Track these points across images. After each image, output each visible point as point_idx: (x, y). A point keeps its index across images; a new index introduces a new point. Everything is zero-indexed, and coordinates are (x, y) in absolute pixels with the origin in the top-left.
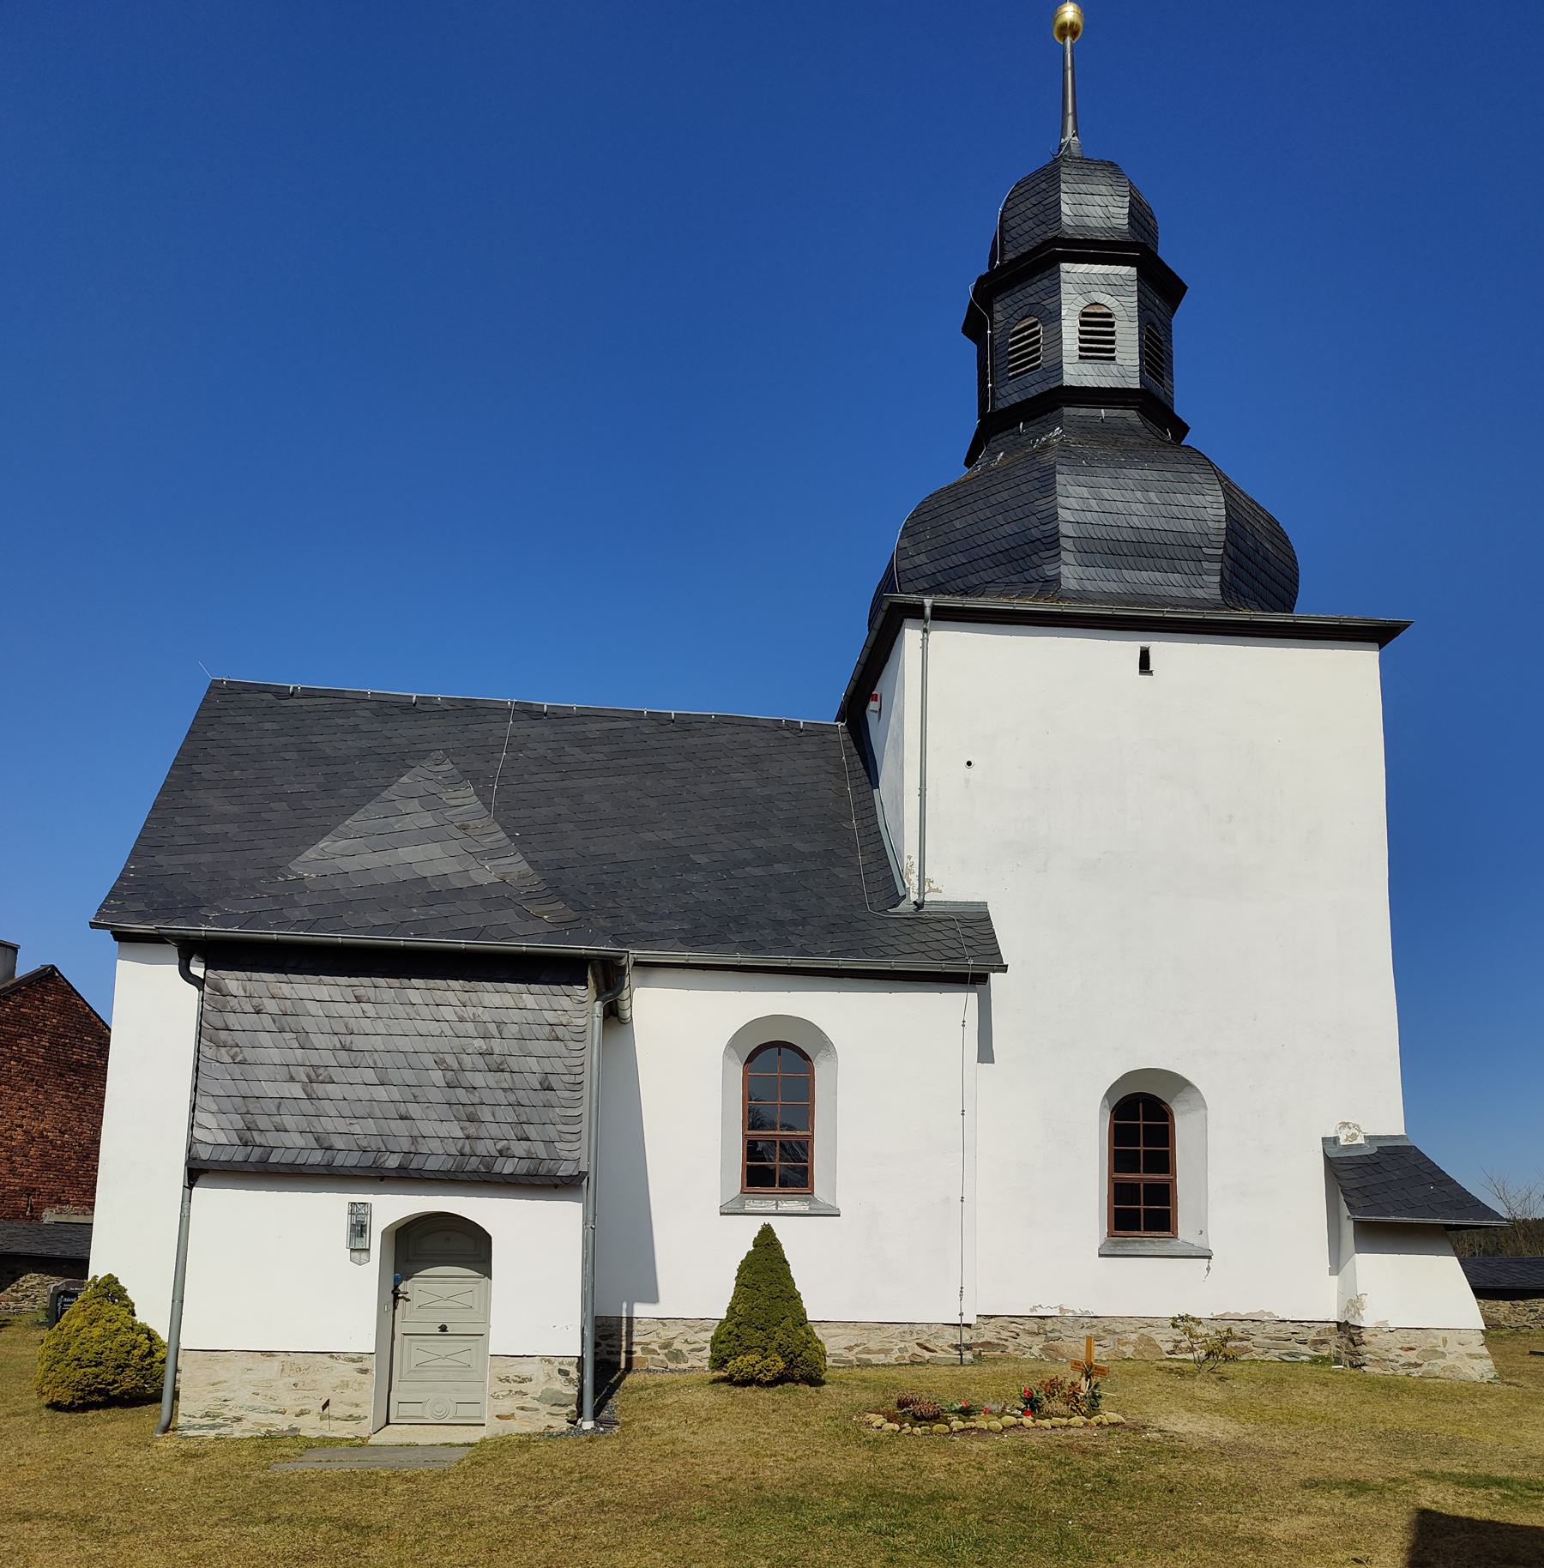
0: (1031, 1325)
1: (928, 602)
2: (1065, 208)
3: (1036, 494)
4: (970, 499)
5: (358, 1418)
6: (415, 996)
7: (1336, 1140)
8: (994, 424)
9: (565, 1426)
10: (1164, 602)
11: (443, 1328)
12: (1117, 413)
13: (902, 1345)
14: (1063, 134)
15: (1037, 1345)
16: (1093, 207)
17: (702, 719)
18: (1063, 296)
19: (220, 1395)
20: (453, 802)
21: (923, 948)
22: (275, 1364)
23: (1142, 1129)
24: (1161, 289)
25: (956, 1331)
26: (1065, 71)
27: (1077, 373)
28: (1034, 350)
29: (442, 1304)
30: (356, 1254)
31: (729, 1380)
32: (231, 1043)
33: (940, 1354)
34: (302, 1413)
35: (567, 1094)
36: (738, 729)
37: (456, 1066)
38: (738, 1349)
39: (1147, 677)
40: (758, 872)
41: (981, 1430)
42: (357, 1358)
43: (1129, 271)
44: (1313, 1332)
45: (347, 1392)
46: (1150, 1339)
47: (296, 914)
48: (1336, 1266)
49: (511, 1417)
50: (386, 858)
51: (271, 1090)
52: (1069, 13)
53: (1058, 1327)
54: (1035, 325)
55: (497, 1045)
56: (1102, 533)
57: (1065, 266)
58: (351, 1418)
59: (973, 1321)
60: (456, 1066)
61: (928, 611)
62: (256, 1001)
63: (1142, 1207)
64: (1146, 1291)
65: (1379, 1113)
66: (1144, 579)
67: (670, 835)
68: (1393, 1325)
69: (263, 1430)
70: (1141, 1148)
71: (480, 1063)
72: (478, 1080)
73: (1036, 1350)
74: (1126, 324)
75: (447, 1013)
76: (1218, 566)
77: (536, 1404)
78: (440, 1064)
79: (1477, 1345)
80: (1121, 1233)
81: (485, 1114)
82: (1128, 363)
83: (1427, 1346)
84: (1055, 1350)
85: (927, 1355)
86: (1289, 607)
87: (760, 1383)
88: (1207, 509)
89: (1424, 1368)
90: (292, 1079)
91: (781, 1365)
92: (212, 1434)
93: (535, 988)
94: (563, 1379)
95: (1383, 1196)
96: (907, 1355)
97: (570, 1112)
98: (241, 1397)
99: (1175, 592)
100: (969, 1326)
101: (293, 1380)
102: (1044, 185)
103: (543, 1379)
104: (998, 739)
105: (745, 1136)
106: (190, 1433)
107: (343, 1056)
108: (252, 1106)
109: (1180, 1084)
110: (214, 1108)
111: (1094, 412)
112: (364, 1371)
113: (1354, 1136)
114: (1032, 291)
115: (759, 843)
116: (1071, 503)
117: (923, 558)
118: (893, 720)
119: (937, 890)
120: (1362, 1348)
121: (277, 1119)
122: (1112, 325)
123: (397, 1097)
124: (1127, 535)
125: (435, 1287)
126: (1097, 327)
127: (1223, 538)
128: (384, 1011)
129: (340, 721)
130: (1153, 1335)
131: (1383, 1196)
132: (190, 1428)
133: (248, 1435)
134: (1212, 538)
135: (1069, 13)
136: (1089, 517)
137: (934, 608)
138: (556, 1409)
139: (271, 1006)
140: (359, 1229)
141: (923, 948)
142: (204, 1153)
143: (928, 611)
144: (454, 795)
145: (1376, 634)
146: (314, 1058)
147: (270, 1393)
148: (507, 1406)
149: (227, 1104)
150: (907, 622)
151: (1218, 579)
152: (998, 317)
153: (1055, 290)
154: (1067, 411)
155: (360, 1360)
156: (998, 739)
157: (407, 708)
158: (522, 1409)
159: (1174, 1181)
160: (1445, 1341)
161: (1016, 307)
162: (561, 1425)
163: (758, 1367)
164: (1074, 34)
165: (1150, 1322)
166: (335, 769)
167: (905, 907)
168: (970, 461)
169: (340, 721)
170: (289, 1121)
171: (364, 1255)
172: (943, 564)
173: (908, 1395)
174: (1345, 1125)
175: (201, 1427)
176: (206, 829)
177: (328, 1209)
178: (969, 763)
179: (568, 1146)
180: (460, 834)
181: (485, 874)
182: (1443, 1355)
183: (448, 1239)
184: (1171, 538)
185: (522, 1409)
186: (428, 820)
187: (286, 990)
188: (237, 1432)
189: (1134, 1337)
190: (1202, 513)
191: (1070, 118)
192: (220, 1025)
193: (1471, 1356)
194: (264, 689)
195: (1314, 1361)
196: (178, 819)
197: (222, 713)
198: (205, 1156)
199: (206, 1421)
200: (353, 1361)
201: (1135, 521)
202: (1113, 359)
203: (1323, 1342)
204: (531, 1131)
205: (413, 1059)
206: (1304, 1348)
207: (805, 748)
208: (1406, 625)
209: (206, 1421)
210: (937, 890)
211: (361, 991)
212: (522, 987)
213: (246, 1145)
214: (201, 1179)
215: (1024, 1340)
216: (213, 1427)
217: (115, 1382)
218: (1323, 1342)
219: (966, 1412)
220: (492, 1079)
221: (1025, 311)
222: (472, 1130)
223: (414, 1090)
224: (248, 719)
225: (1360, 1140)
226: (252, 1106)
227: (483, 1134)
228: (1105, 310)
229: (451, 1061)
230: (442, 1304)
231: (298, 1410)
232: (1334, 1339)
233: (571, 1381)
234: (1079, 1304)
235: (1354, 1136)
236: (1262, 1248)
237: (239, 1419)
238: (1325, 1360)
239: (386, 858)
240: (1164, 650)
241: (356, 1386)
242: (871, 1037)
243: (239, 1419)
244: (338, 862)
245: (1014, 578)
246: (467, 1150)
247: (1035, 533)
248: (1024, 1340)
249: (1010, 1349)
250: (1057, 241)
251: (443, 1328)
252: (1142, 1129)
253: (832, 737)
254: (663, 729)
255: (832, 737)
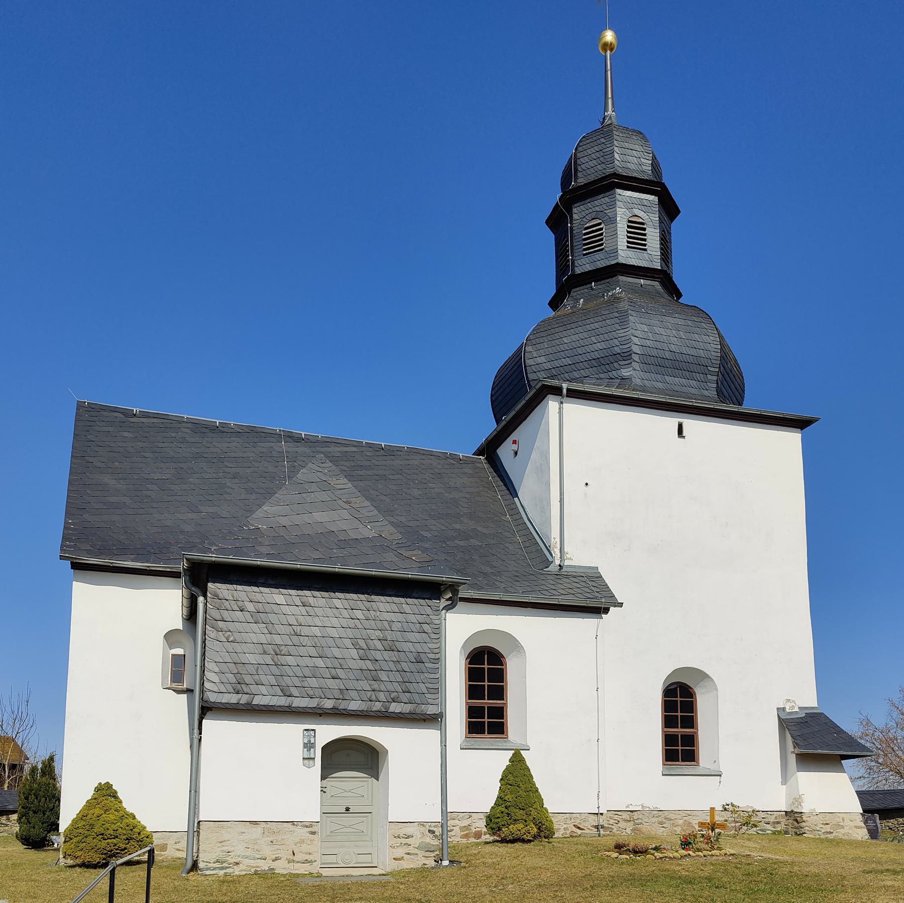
0: (626, 816)
1: (565, 386)
2: (616, 156)
3: (617, 326)
4: (573, 326)
5: (311, 862)
6: (337, 603)
7: (784, 709)
8: (568, 282)
9: (434, 864)
10: (688, 396)
11: (347, 809)
12: (648, 282)
13: (565, 826)
14: (606, 110)
15: (629, 827)
16: (631, 158)
17: (400, 449)
18: (618, 209)
19: (225, 848)
20: (339, 487)
21: (571, 591)
22: (259, 829)
23: (679, 703)
24: (669, 209)
25: (595, 817)
26: (606, 72)
27: (627, 256)
28: (595, 242)
29: (345, 794)
30: (306, 761)
31: (504, 841)
32: (225, 629)
33: (587, 831)
34: (276, 859)
35: (431, 665)
36: (423, 457)
37: (365, 647)
38: (509, 822)
39: (682, 440)
40: (462, 543)
41: (670, 858)
42: (309, 825)
43: (653, 198)
44: (773, 817)
45: (304, 846)
46: (690, 823)
47: (264, 550)
48: (785, 780)
49: (402, 859)
50: (306, 518)
51: (252, 659)
52: (609, 36)
53: (641, 816)
54: (600, 224)
55: (389, 635)
56: (654, 352)
57: (619, 191)
58: (306, 861)
59: (605, 812)
60: (365, 647)
61: (565, 391)
62: (240, 603)
63: (680, 748)
64: (688, 797)
65: (805, 696)
66: (676, 381)
67: (403, 520)
68: (818, 811)
69: (253, 870)
70: (679, 714)
71: (379, 645)
72: (378, 655)
73: (629, 831)
74: (653, 230)
75: (359, 614)
76: (715, 378)
77: (416, 851)
78: (356, 646)
79: (859, 821)
80: (669, 763)
81: (383, 676)
82: (654, 253)
83: (835, 823)
84: (639, 830)
85: (579, 832)
86: (740, 404)
87: (524, 841)
88: (708, 346)
89: (834, 834)
90: (265, 653)
91: (536, 830)
92: (222, 873)
93: (409, 600)
94: (431, 836)
95: (813, 741)
96: (568, 832)
97: (432, 676)
98: (239, 850)
99: (693, 391)
100: (602, 814)
101: (271, 839)
102: (603, 140)
103: (419, 836)
104: (598, 470)
105: (467, 703)
106: (208, 872)
107: (295, 638)
108: (241, 669)
109: (702, 676)
110: (217, 670)
111: (636, 281)
112: (313, 833)
113: (793, 707)
114: (600, 202)
115: (457, 526)
116: (638, 333)
117: (543, 359)
118: (535, 456)
119: (570, 559)
120: (803, 824)
121: (256, 677)
122: (644, 229)
123: (330, 665)
124: (668, 355)
125: (350, 782)
126: (636, 231)
127: (718, 362)
128: (319, 612)
129: (173, 435)
130: (691, 821)
131: (813, 741)
132: (208, 869)
133: (243, 873)
134: (714, 361)
135: (609, 36)
136: (648, 343)
137: (568, 390)
138: (428, 854)
139: (250, 607)
140: (309, 746)
141: (571, 591)
142: (212, 697)
143: (565, 391)
144: (338, 482)
145: (799, 424)
146: (278, 639)
147: (256, 847)
148: (399, 852)
149: (224, 667)
150: (550, 396)
151: (715, 385)
152: (575, 216)
153: (613, 205)
154: (622, 278)
155: (311, 826)
156: (598, 470)
157: (213, 429)
158: (408, 854)
159: (696, 733)
160: (843, 820)
161: (587, 212)
162: (431, 863)
163: (523, 831)
164: (611, 50)
165: (689, 813)
166: (181, 465)
167: (553, 568)
168: (555, 303)
169: (173, 435)
170: (264, 679)
171: (311, 762)
172: (556, 364)
173: (621, 841)
174: (788, 700)
175: (215, 869)
176: (112, 499)
177: (291, 733)
178: (587, 484)
179: (433, 696)
180: (347, 507)
181: (368, 532)
182: (843, 827)
183: (348, 755)
184: (691, 359)
185: (408, 854)
186: (324, 496)
187: (259, 597)
188: (237, 871)
189: (681, 822)
190: (708, 347)
191: (610, 101)
192: (219, 617)
193: (856, 827)
194: (115, 410)
195: (774, 833)
196: (88, 491)
197: (92, 424)
198: (212, 700)
199: (217, 865)
200: (307, 827)
201: (673, 348)
202: (645, 250)
203: (778, 823)
204: (411, 687)
205: (338, 641)
206: (768, 827)
207: (466, 471)
208: (817, 420)
209: (217, 865)
210: (570, 559)
211: (304, 599)
212: (402, 600)
213: (238, 693)
214: (209, 714)
215: (622, 824)
216: (222, 868)
217: (125, 849)
218: (778, 823)
219: (656, 849)
220: (387, 655)
221: (593, 215)
222: (375, 685)
223: (340, 661)
224: (110, 429)
225: (796, 709)
226: (241, 669)
227: (383, 688)
228: (641, 220)
229: (362, 643)
230: (345, 794)
231: (274, 857)
232: (783, 821)
233: (436, 836)
234: (652, 804)
235: (793, 707)
236: (745, 769)
237: (237, 864)
238: (779, 832)
239: (306, 518)
240: (692, 424)
241: (309, 842)
242: (540, 646)
243: (237, 864)
244: (278, 519)
245: (602, 376)
246: (374, 698)
247: (617, 350)
248: (622, 824)
249: (615, 830)
250: (615, 175)
251: (347, 809)
252: (679, 703)
253: (479, 465)
254: (378, 454)
255: (479, 465)
